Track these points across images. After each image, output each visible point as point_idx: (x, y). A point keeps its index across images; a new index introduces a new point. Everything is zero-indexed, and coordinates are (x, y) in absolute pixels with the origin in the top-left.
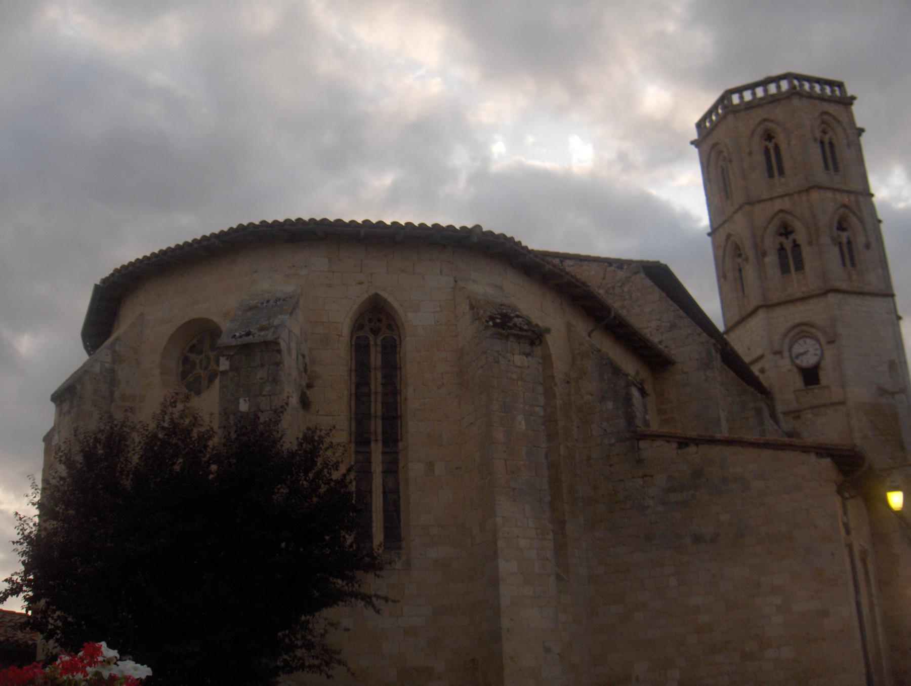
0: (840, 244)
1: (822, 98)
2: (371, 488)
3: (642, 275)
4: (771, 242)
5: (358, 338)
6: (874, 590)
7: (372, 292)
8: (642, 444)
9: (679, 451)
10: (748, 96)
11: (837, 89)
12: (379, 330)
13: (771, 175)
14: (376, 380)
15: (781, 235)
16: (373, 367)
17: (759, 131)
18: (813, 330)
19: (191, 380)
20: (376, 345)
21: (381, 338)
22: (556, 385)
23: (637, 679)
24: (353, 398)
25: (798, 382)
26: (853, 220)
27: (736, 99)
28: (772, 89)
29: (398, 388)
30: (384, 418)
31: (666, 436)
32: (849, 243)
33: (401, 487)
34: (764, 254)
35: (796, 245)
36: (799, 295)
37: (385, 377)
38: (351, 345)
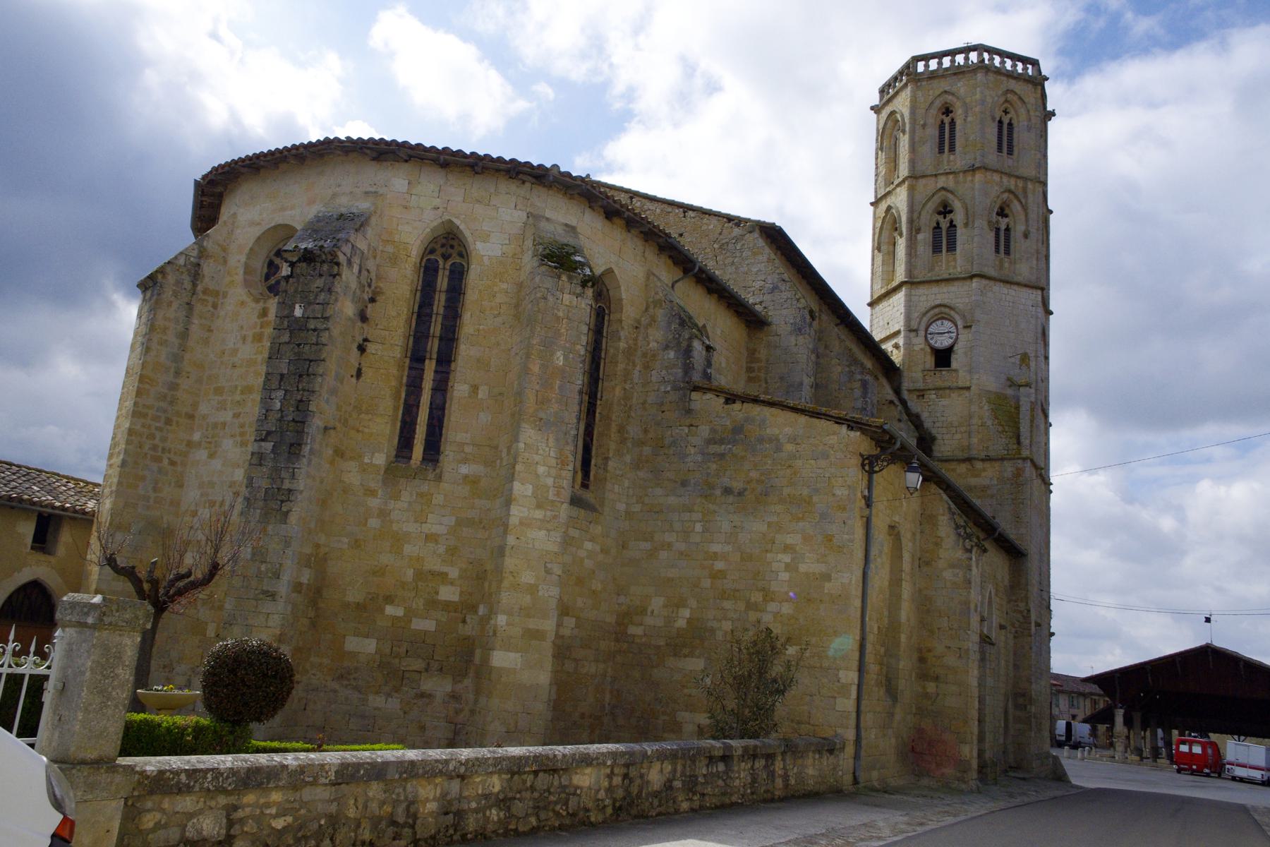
0: (998, 230)
1: (1012, 75)
2: (419, 402)
3: (756, 234)
4: (928, 218)
5: (429, 260)
6: (906, 566)
7: (446, 217)
8: (695, 395)
9: (726, 407)
10: (933, 64)
11: (1030, 67)
12: (450, 256)
13: (941, 151)
14: (440, 301)
15: (940, 213)
16: (438, 289)
17: (938, 103)
18: (952, 313)
19: (273, 282)
20: (444, 269)
21: (450, 263)
22: (623, 328)
23: (652, 612)
24: (415, 316)
25: (930, 361)
26: (1016, 206)
27: (921, 67)
28: (960, 59)
29: (459, 312)
30: (441, 339)
31: (716, 391)
32: (1007, 229)
33: (447, 405)
34: (918, 231)
35: (952, 225)
36: (946, 276)
37: (448, 300)
38: (421, 266)
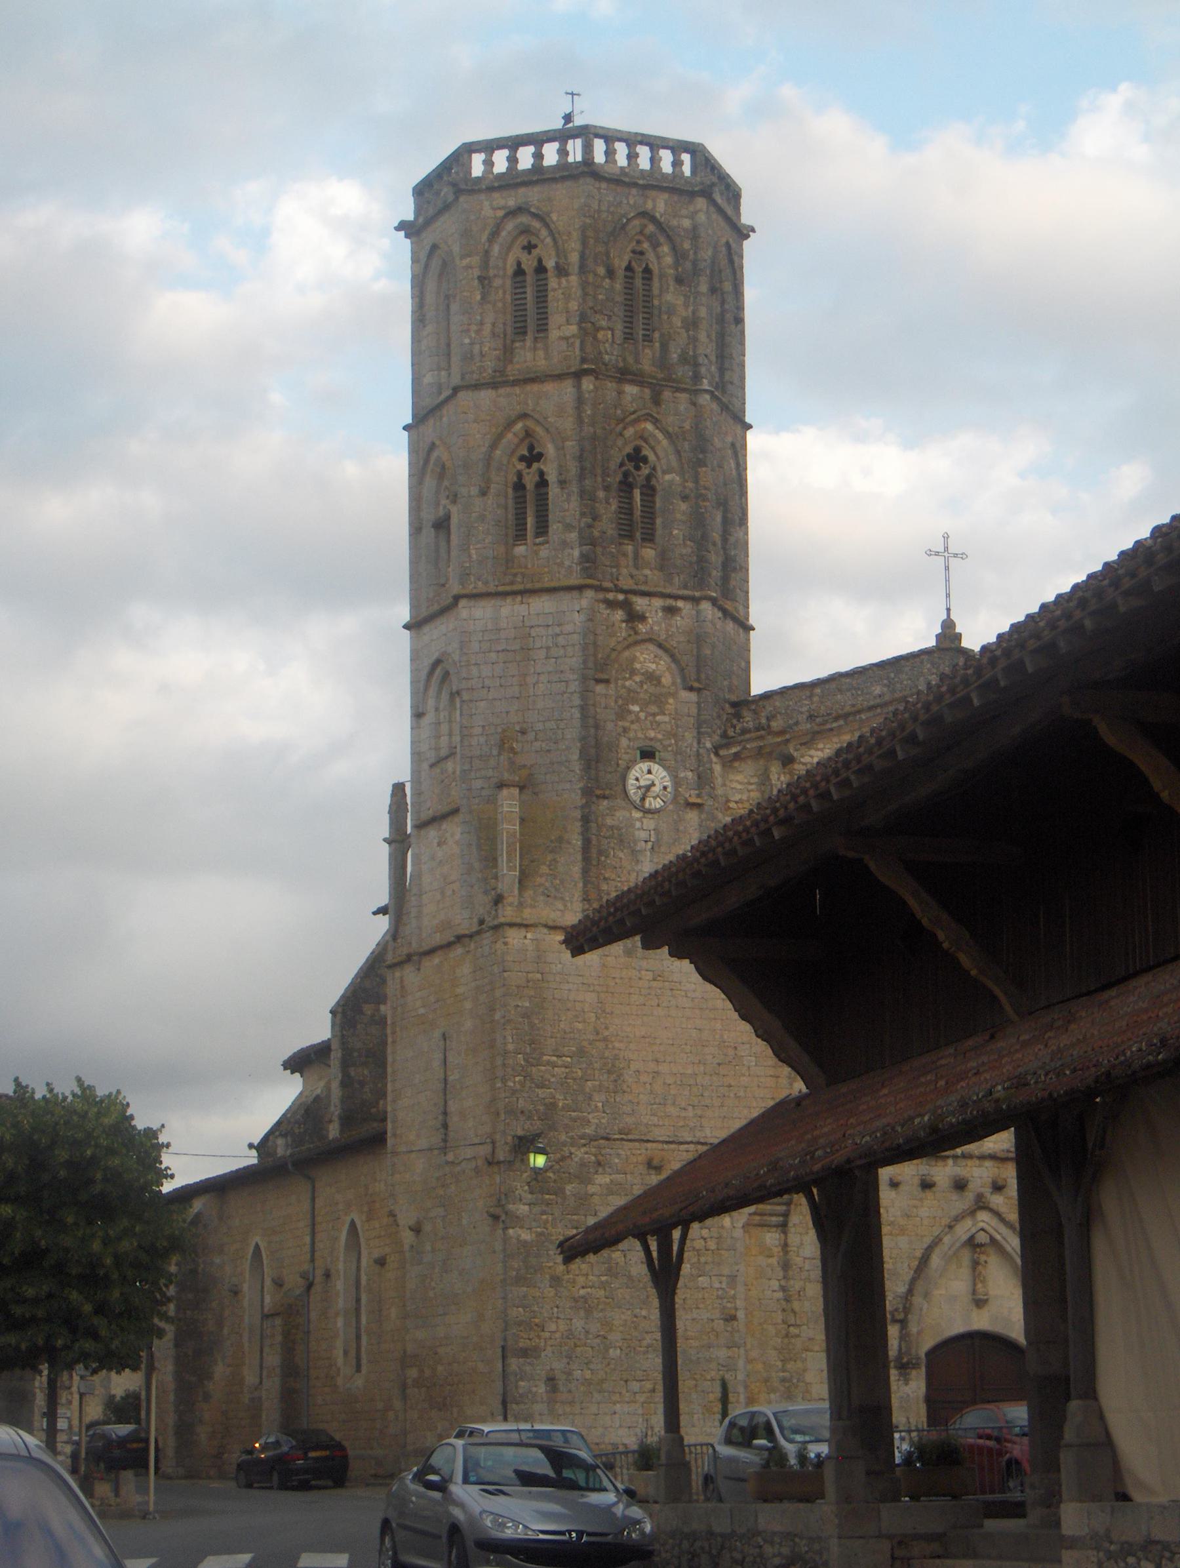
27: (477, 167)
35: (543, 483)
